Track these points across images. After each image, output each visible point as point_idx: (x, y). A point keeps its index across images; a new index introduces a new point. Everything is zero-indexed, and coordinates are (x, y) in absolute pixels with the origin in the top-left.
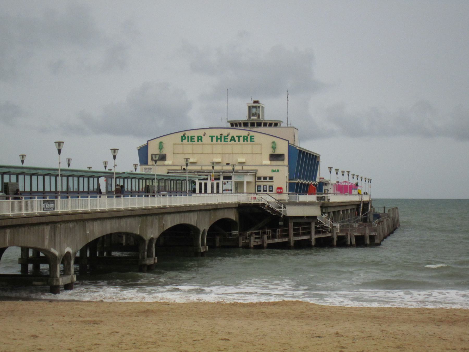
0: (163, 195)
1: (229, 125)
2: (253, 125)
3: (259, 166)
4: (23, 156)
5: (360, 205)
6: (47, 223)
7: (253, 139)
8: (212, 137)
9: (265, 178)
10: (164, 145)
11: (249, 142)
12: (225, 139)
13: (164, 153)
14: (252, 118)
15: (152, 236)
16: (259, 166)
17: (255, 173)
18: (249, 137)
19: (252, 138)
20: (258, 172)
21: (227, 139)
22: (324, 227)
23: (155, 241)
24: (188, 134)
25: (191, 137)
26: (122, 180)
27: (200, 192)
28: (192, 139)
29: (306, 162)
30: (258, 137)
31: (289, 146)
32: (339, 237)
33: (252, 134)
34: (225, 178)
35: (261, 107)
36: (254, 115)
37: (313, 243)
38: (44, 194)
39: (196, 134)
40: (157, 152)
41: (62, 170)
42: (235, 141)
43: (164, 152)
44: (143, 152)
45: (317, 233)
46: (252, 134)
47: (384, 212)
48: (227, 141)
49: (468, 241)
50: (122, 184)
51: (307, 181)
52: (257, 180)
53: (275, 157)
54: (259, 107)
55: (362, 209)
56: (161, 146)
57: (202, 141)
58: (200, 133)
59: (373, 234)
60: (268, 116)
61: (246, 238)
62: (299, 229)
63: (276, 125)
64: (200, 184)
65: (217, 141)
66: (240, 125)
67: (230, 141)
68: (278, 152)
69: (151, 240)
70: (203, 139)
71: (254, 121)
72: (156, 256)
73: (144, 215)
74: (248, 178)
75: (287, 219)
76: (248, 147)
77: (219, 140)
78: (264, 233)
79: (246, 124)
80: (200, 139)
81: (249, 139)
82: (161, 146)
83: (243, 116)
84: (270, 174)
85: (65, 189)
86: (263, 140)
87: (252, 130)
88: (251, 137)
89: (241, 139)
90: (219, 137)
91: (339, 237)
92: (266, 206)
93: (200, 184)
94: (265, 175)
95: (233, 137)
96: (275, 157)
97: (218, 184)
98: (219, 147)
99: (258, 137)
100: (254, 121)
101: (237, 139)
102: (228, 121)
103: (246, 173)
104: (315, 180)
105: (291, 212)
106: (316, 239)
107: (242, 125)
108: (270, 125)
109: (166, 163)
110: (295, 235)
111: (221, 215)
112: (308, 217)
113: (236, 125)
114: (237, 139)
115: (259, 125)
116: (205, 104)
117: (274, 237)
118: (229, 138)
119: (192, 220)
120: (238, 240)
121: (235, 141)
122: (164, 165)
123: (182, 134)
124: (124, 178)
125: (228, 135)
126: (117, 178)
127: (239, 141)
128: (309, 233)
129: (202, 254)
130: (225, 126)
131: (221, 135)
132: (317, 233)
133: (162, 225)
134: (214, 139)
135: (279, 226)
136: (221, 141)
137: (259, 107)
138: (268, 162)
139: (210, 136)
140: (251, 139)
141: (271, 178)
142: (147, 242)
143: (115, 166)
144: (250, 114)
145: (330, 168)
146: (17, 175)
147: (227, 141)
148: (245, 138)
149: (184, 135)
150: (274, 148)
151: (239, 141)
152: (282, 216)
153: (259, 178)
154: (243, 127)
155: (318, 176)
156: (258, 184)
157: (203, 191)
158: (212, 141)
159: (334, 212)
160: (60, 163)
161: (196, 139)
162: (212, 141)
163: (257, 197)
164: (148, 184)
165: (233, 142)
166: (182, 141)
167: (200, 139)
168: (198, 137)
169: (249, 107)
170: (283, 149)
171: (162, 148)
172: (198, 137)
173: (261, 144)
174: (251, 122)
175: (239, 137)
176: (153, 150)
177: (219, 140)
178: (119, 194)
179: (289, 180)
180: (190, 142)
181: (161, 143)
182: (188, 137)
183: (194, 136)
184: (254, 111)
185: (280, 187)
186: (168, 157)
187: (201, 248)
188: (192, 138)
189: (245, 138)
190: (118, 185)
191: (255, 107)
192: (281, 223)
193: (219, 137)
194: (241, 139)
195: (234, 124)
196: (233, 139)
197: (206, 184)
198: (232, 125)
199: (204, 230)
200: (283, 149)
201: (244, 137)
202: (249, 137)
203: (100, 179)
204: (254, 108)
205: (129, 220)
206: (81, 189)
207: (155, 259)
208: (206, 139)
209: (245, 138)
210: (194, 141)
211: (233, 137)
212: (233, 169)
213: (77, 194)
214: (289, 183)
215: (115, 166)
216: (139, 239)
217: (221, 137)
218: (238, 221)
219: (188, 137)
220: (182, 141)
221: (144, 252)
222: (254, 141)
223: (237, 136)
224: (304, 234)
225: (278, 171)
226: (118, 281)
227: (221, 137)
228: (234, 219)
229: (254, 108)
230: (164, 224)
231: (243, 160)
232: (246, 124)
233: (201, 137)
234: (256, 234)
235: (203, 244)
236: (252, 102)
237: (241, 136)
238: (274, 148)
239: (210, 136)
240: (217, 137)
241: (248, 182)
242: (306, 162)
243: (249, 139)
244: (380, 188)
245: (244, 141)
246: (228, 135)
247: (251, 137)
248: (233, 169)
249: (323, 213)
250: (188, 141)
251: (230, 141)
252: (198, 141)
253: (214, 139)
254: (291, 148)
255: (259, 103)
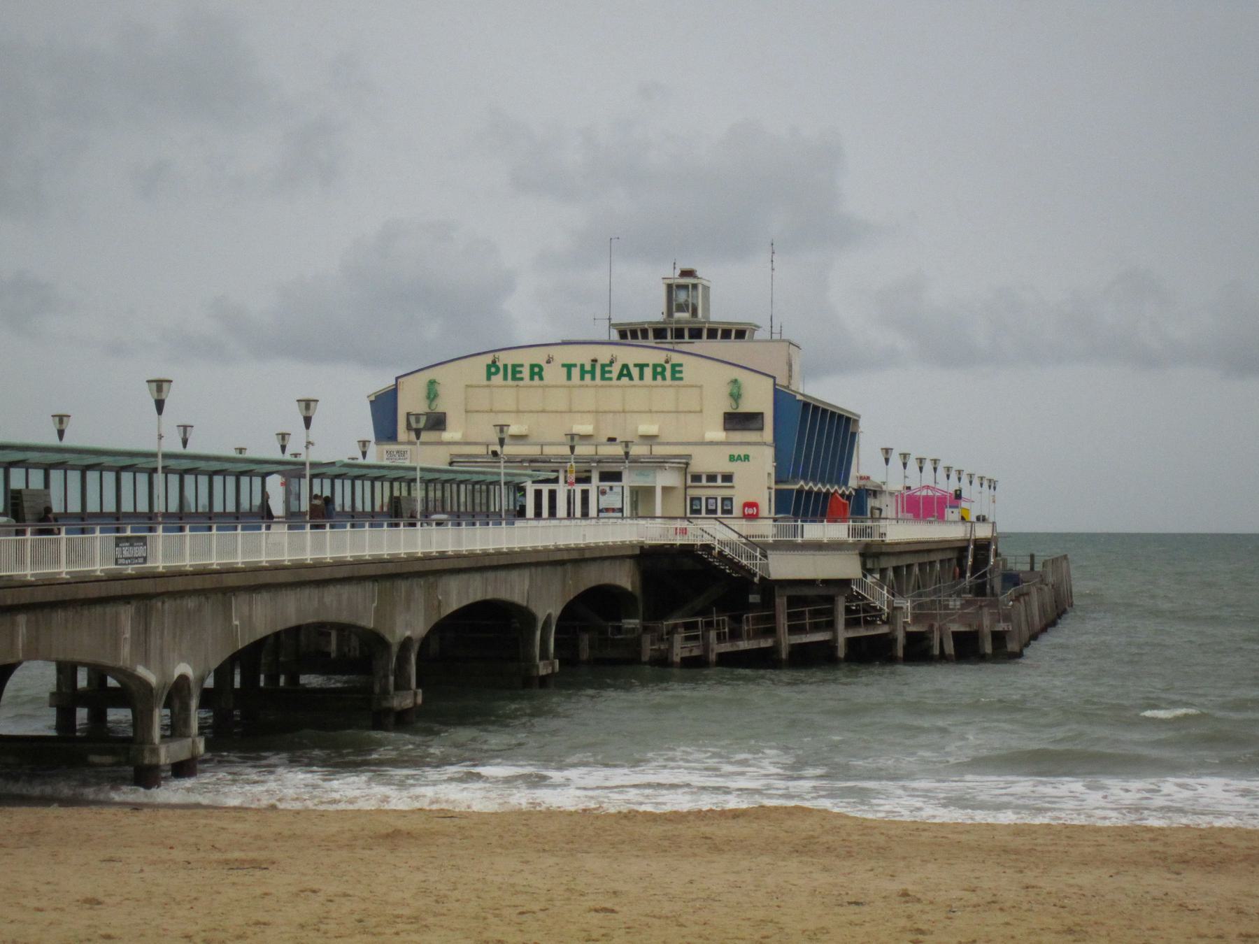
0: (439, 524)
1: (615, 336)
2: (679, 334)
3: (696, 444)
4: (61, 418)
5: (965, 549)
6: (126, 599)
7: (681, 372)
8: (569, 367)
9: (711, 478)
10: (441, 390)
11: (669, 381)
12: (603, 372)
13: (440, 409)
14: (678, 315)
15: (408, 633)
16: (696, 444)
17: (683, 464)
18: (668, 366)
19: (676, 370)
20: (692, 462)
21: (610, 372)
22: (869, 608)
23: (416, 647)
24: (506, 359)
25: (514, 366)
26: (327, 482)
27: (538, 514)
28: (514, 372)
29: (821, 435)
30: (692, 368)
31: (776, 391)
32: (909, 635)
33: (676, 358)
34: (605, 477)
35: (700, 288)
36: (681, 308)
37: (841, 653)
38: (118, 519)
39: (526, 359)
40: (421, 407)
41: (166, 456)
42: (631, 378)
43: (440, 407)
44: (384, 407)
45: (850, 623)
46: (676, 358)
47: (1032, 569)
48: (610, 379)
49: (1257, 647)
50: (327, 493)
51: (824, 485)
52: (689, 483)
53: (738, 421)
54: (695, 286)
55: (972, 561)
56: (432, 392)
57: (541, 378)
58: (538, 356)
59: (1001, 626)
60: (719, 312)
61: (661, 639)
62: (803, 613)
63: (741, 334)
64: (538, 494)
65: (582, 378)
66: (645, 336)
67: (619, 378)
68: (747, 406)
69: (406, 644)
70: (543, 373)
71: (682, 325)
72: (418, 686)
73: (388, 576)
74: (666, 479)
75: (770, 587)
76: (665, 395)
77: (588, 377)
78: (709, 625)
79: (660, 333)
80: (536, 371)
81: (668, 374)
82: (432, 392)
83: (653, 311)
84: (723, 466)
85: (173, 507)
86: (707, 377)
87: (678, 347)
88: (674, 366)
89: (648, 372)
90: (588, 368)
91: (909, 635)
92: (715, 552)
93: (538, 494)
94: (712, 469)
95: (625, 366)
96: (738, 421)
97: (585, 494)
98: (589, 395)
99: (692, 368)
100: (682, 325)
101: (635, 372)
102: (612, 325)
103: (660, 463)
104: (846, 483)
105: (782, 567)
106: (850, 641)
107: (651, 334)
108: (726, 334)
109: (447, 436)
110: (793, 630)
111: (593, 577)
112: (826, 582)
113: (634, 335)
114: (635, 372)
115: (696, 334)
116: (550, 279)
117: (735, 635)
118: (616, 369)
119: (515, 589)
120: (638, 643)
121: (631, 378)
122: (441, 443)
123: (488, 359)
124: (333, 478)
125: (612, 362)
126: (313, 476)
127: (641, 378)
128: (830, 625)
129: (544, 682)
130: (605, 338)
131: (595, 361)
132: (850, 623)
133: (436, 603)
134: (576, 372)
135: (750, 607)
136: (593, 378)
137: (695, 286)
138: (720, 435)
139: (563, 365)
140: (674, 372)
141: (728, 478)
142: (395, 649)
143: (309, 444)
144: (672, 305)
145: (887, 451)
146: (47, 468)
147: (610, 379)
148: (659, 370)
149: (494, 362)
150: (736, 397)
151: (641, 378)
152: (756, 580)
153: (696, 478)
154: (651, 341)
155: (853, 472)
156: (693, 492)
157: (545, 512)
158: (569, 377)
159: (897, 570)
160: (160, 437)
161: (526, 372)
162: (569, 377)
163: (690, 527)
164: (396, 493)
165: (625, 380)
166: (489, 378)
167: (536, 371)
168: (532, 367)
169: (670, 287)
170: (759, 399)
171: (436, 396)
172: (532, 367)
173: (701, 387)
174: (674, 326)
175: (641, 367)
176: (411, 402)
177: (588, 377)
178: (319, 521)
179: (777, 482)
180: (510, 382)
181: (432, 383)
182: (505, 366)
183: (522, 366)
184: (682, 296)
185: (751, 500)
186: (450, 421)
187: (541, 664)
188: (515, 371)
189: (658, 371)
190: (316, 497)
191: (685, 287)
192: (754, 598)
193: (588, 368)
194: (648, 372)
195: (629, 334)
196: (625, 372)
197: (552, 494)
198: (623, 335)
199: (549, 616)
200: (759, 399)
201: (655, 366)
202: (668, 366)
203: (269, 480)
204: (683, 289)
205: (346, 591)
206: (218, 508)
207: (416, 694)
208: (553, 374)
209: (536, 370)
210: (522, 379)
211: (625, 366)
212: (627, 454)
213: (208, 519)
214: (777, 491)
215: (309, 444)
216: (373, 642)
217: (593, 367)
218: (638, 593)
219: (505, 366)
220: (489, 378)
221: (386, 677)
222: (681, 379)
223: (636, 365)
224: (816, 628)
225: (747, 458)
226: (317, 752)
227: (593, 367)
228: (630, 589)
229: (683, 289)
230: (440, 602)
231: (652, 429)
232: (660, 333)
233: (541, 368)
234: (688, 626)
235: (544, 655)
236: (678, 272)
237: (647, 365)
238: (736, 397)
239: (563, 365)
240: (582, 366)
241: (665, 489)
242: (821, 435)
243: (668, 374)
244: (1020, 506)
245: (655, 378)
246: (612, 362)
247: (674, 366)
248: (627, 454)
249: (867, 571)
250: (505, 378)
251: (619, 378)
252: (532, 378)
253: (576, 372)
254: (782, 397)
255: (696, 277)
